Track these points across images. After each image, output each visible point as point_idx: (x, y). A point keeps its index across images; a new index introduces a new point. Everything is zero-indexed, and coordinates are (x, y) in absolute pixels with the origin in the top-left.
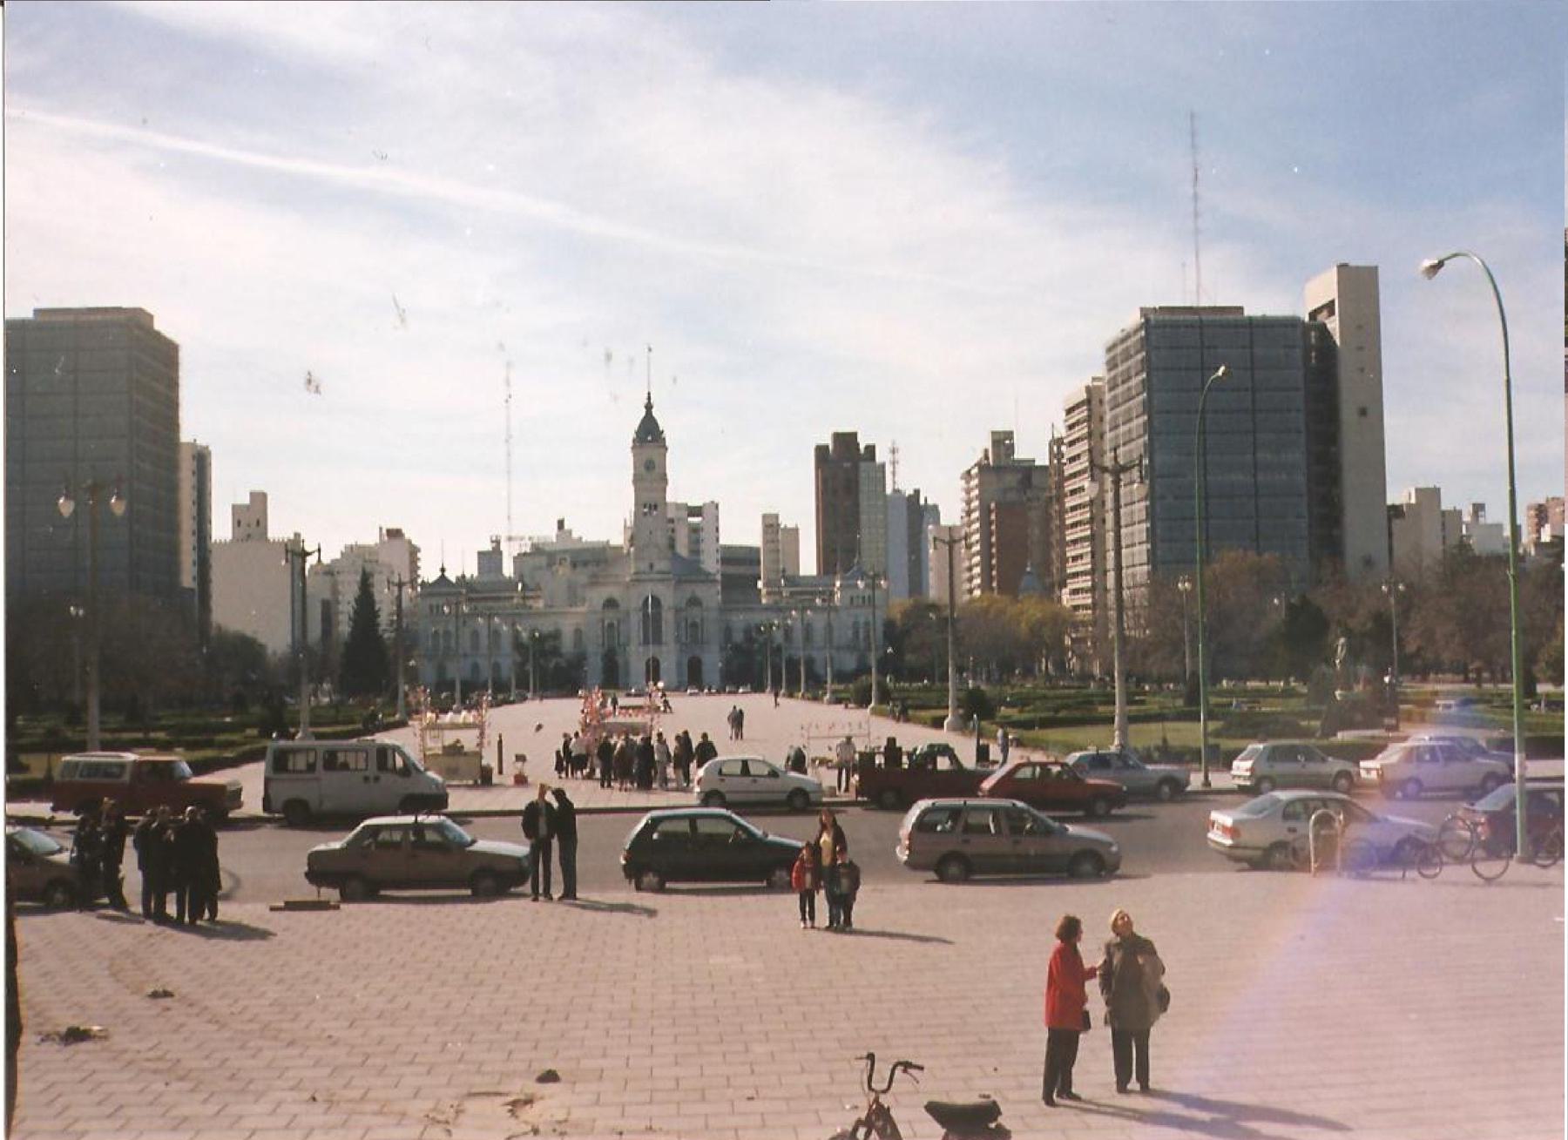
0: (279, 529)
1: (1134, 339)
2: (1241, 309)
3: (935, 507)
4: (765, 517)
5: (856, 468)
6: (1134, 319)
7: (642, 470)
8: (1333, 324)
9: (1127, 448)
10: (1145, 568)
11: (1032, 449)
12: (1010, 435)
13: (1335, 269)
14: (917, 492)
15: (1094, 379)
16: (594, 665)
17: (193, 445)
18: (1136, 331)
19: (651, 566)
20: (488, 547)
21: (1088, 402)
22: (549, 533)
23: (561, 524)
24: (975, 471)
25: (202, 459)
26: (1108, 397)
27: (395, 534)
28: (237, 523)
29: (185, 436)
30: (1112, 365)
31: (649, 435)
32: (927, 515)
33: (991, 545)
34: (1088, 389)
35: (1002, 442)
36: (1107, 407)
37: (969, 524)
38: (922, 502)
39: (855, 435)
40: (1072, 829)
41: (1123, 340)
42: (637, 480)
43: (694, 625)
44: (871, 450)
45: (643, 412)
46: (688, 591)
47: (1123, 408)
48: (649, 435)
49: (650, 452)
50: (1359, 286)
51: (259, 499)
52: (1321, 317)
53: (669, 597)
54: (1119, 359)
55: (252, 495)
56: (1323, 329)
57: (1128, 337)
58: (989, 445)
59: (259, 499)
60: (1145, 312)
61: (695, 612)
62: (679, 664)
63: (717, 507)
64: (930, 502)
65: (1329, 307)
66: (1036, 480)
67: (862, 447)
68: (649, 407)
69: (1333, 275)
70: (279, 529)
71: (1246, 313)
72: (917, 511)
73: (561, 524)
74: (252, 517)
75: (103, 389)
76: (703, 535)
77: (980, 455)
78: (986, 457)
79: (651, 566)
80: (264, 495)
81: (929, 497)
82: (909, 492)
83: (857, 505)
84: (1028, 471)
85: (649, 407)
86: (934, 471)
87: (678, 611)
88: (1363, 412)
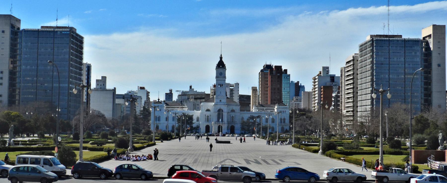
0: (109, 86)
1: (368, 44)
2: (401, 36)
3: (304, 86)
4: (252, 87)
5: (281, 75)
6: (368, 38)
7: (219, 75)
8: (431, 41)
9: (361, 64)
10: (370, 106)
11: (335, 71)
12: (328, 68)
13: (432, 26)
14: (298, 82)
15: (355, 54)
16: (203, 129)
17: (86, 64)
18: (369, 42)
19: (220, 101)
20: (168, 92)
21: (353, 60)
22: (188, 89)
23: (191, 87)
24: (317, 77)
25: (89, 68)
26: (360, 59)
27: (142, 88)
28: (97, 85)
29: (85, 61)
30: (361, 51)
31: (221, 65)
32: (301, 89)
33: (321, 98)
34: (353, 57)
35: (326, 69)
36: (359, 62)
37: (315, 92)
38: (300, 85)
39: (281, 66)
40: (86, 12)
41: (365, 44)
42: (217, 77)
43: (233, 117)
44: (286, 71)
45: (219, 60)
46: (231, 108)
47: (364, 63)
48: (221, 65)
49: (221, 70)
50: (439, 30)
51: (104, 78)
52: (427, 39)
53: (225, 109)
54: (367, 58)
55: (102, 77)
56: (427, 44)
57: (366, 43)
58: (321, 70)
59: (104, 78)
60: (372, 36)
61: (233, 114)
62: (228, 127)
63: (238, 84)
64: (302, 85)
65: (430, 36)
66: (335, 80)
67: (283, 70)
68: (221, 58)
69: (431, 28)
70: (109, 86)
71: (403, 37)
72: (298, 88)
73: (191, 87)
74: (102, 81)
75: (12, 22)
76: (234, 92)
77: (319, 73)
78: (320, 73)
79: (220, 101)
80: (106, 77)
81: (302, 83)
82: (296, 82)
83: (281, 86)
84: (333, 78)
85: (221, 58)
86: (303, 74)
87: (228, 113)
88: (439, 65)
